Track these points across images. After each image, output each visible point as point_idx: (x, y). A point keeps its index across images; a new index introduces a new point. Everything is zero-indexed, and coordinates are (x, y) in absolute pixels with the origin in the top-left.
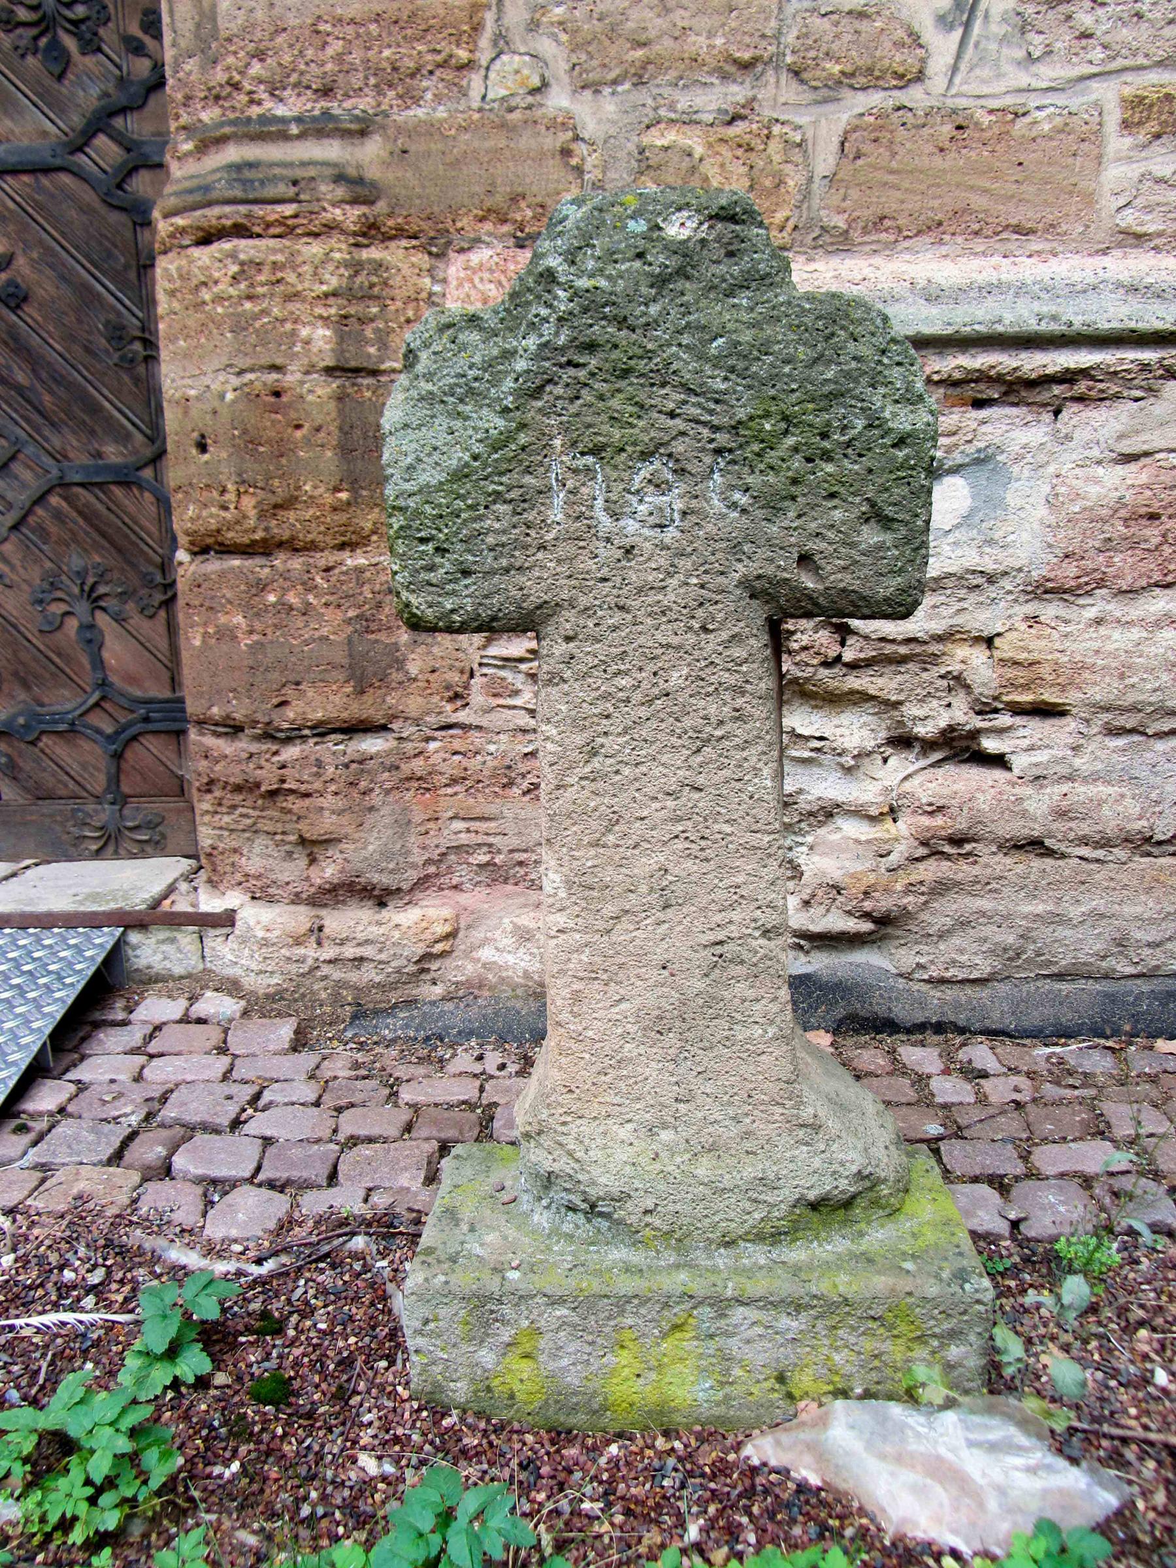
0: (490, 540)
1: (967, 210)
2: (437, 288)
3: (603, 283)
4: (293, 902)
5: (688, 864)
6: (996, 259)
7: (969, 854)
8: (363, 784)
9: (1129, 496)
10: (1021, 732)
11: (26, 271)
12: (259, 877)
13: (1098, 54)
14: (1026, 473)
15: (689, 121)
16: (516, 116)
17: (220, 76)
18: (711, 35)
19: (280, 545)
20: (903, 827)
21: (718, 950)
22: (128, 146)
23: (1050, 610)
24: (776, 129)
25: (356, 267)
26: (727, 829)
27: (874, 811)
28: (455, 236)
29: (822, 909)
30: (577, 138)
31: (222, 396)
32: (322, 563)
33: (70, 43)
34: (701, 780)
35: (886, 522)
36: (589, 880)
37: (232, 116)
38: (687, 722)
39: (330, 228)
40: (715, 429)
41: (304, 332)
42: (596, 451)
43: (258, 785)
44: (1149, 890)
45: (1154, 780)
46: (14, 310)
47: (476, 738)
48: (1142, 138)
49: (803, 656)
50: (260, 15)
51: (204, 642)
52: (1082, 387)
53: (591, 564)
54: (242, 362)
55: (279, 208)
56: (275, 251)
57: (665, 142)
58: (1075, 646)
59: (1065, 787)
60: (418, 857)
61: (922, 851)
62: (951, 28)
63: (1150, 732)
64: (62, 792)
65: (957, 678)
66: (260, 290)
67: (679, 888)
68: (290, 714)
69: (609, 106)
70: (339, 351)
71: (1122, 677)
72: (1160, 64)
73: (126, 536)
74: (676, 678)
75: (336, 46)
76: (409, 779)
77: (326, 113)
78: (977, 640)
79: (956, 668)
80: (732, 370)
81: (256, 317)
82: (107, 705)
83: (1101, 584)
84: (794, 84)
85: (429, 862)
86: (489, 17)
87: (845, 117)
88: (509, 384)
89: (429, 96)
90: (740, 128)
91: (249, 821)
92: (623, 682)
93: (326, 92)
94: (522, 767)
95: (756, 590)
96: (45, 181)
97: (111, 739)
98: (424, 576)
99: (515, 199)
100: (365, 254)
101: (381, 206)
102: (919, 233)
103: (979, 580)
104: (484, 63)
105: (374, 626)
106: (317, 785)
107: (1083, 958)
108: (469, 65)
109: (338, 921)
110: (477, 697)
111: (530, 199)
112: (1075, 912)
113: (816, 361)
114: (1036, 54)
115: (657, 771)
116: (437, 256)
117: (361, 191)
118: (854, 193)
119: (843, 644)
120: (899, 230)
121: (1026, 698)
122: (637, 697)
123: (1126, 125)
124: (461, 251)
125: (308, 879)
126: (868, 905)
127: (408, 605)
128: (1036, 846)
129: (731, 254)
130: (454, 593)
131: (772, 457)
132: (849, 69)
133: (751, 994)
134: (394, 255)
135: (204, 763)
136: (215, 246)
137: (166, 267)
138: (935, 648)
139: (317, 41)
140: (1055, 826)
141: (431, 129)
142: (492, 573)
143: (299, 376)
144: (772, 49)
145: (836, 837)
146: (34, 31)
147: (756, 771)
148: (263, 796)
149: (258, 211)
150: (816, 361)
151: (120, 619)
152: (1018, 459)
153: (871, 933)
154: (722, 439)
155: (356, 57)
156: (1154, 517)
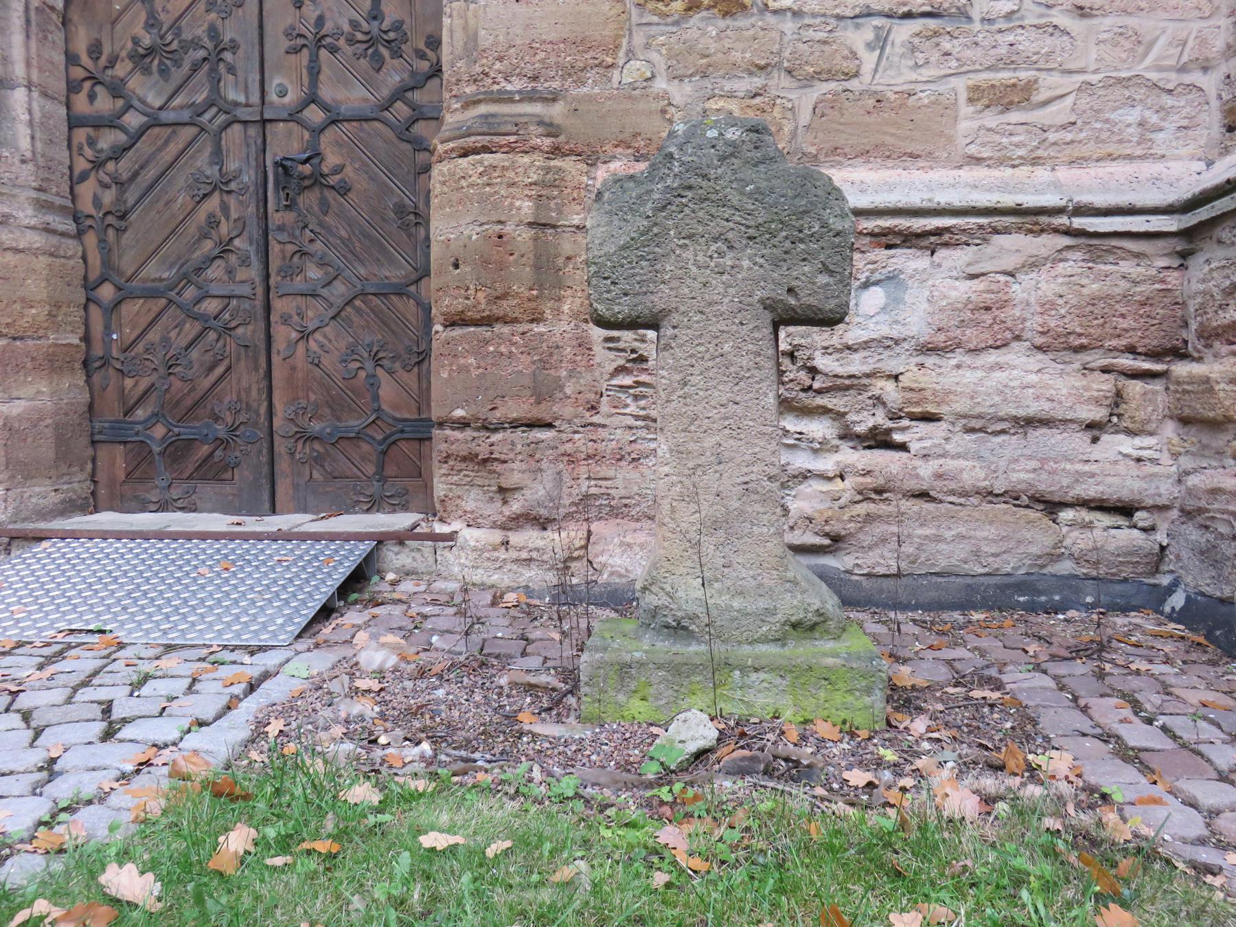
0: (638, 278)
1: (883, 144)
2: (590, 182)
3: (695, 159)
5: (731, 442)
6: (900, 171)
7: (886, 499)
8: (537, 456)
9: (974, 297)
10: (915, 430)
11: (351, 175)
13: (954, 64)
14: (916, 285)
15: (731, 95)
16: (637, 92)
17: (478, 69)
18: (743, 52)
19: (497, 319)
20: (848, 483)
21: (746, 486)
23: (930, 361)
24: (778, 101)
25: (548, 170)
26: (751, 423)
27: (831, 474)
28: (601, 155)
29: (801, 531)
30: (670, 104)
31: (470, 237)
32: (521, 330)
33: (385, 52)
34: (738, 399)
35: (831, 273)
36: (682, 448)
37: (482, 90)
38: (732, 369)
39: (534, 148)
40: (748, 227)
41: (518, 203)
42: (690, 237)
43: (477, 456)
44: (991, 523)
45: (992, 459)
46: (342, 196)
47: (602, 433)
48: (979, 106)
49: (791, 385)
50: (501, 38)
52: (946, 237)
53: (686, 291)
54: (483, 219)
56: (503, 160)
57: (717, 107)
58: (945, 380)
59: (942, 461)
60: (566, 501)
61: (859, 497)
62: (873, 49)
63: (989, 430)
64: (349, 473)
65: (878, 398)
66: (495, 181)
67: (726, 454)
68: (498, 414)
69: (688, 88)
70: (536, 214)
71: (972, 398)
72: (988, 69)
73: (397, 324)
74: (727, 347)
75: (542, 55)
76: (563, 455)
77: (534, 89)
78: (889, 377)
79: (877, 392)
80: (756, 200)
81: (492, 195)
82: (379, 422)
83: (959, 345)
84: (789, 78)
85: (573, 504)
86: (625, 42)
87: (816, 95)
88: (650, 205)
90: (758, 100)
92: (702, 349)
93: (535, 78)
94: (628, 449)
95: (768, 305)
96: (365, 125)
97: (380, 443)
98: (605, 295)
99: (635, 135)
100: (552, 163)
101: (562, 138)
102: (857, 156)
103: (890, 343)
104: (621, 64)
105: (547, 366)
106: (511, 456)
107: (954, 562)
108: (612, 66)
109: (516, 538)
110: (605, 407)
111: (643, 136)
112: (948, 534)
113: (796, 196)
114: (920, 63)
115: (717, 393)
116: (591, 165)
117: (550, 129)
118: (820, 135)
119: (813, 379)
120: (846, 155)
121: (917, 410)
122: (707, 356)
123: (971, 100)
124: (605, 162)
125: (501, 513)
126: (827, 529)
127: (596, 310)
128: (923, 495)
129: (756, 148)
130: (619, 304)
131: (775, 241)
132: (818, 70)
133: (762, 510)
134: (568, 164)
135: (445, 445)
136: (471, 158)
137: (440, 171)
138: (865, 381)
139: (532, 52)
140: (935, 483)
141: (590, 99)
142: (638, 294)
144: (776, 59)
145: (809, 490)
146: (366, 46)
147: (766, 395)
148: (478, 464)
149: (496, 139)
150: (796, 196)
151: (391, 372)
152: (911, 277)
153: (829, 546)
154: (751, 232)
155: (552, 60)
156: (988, 309)
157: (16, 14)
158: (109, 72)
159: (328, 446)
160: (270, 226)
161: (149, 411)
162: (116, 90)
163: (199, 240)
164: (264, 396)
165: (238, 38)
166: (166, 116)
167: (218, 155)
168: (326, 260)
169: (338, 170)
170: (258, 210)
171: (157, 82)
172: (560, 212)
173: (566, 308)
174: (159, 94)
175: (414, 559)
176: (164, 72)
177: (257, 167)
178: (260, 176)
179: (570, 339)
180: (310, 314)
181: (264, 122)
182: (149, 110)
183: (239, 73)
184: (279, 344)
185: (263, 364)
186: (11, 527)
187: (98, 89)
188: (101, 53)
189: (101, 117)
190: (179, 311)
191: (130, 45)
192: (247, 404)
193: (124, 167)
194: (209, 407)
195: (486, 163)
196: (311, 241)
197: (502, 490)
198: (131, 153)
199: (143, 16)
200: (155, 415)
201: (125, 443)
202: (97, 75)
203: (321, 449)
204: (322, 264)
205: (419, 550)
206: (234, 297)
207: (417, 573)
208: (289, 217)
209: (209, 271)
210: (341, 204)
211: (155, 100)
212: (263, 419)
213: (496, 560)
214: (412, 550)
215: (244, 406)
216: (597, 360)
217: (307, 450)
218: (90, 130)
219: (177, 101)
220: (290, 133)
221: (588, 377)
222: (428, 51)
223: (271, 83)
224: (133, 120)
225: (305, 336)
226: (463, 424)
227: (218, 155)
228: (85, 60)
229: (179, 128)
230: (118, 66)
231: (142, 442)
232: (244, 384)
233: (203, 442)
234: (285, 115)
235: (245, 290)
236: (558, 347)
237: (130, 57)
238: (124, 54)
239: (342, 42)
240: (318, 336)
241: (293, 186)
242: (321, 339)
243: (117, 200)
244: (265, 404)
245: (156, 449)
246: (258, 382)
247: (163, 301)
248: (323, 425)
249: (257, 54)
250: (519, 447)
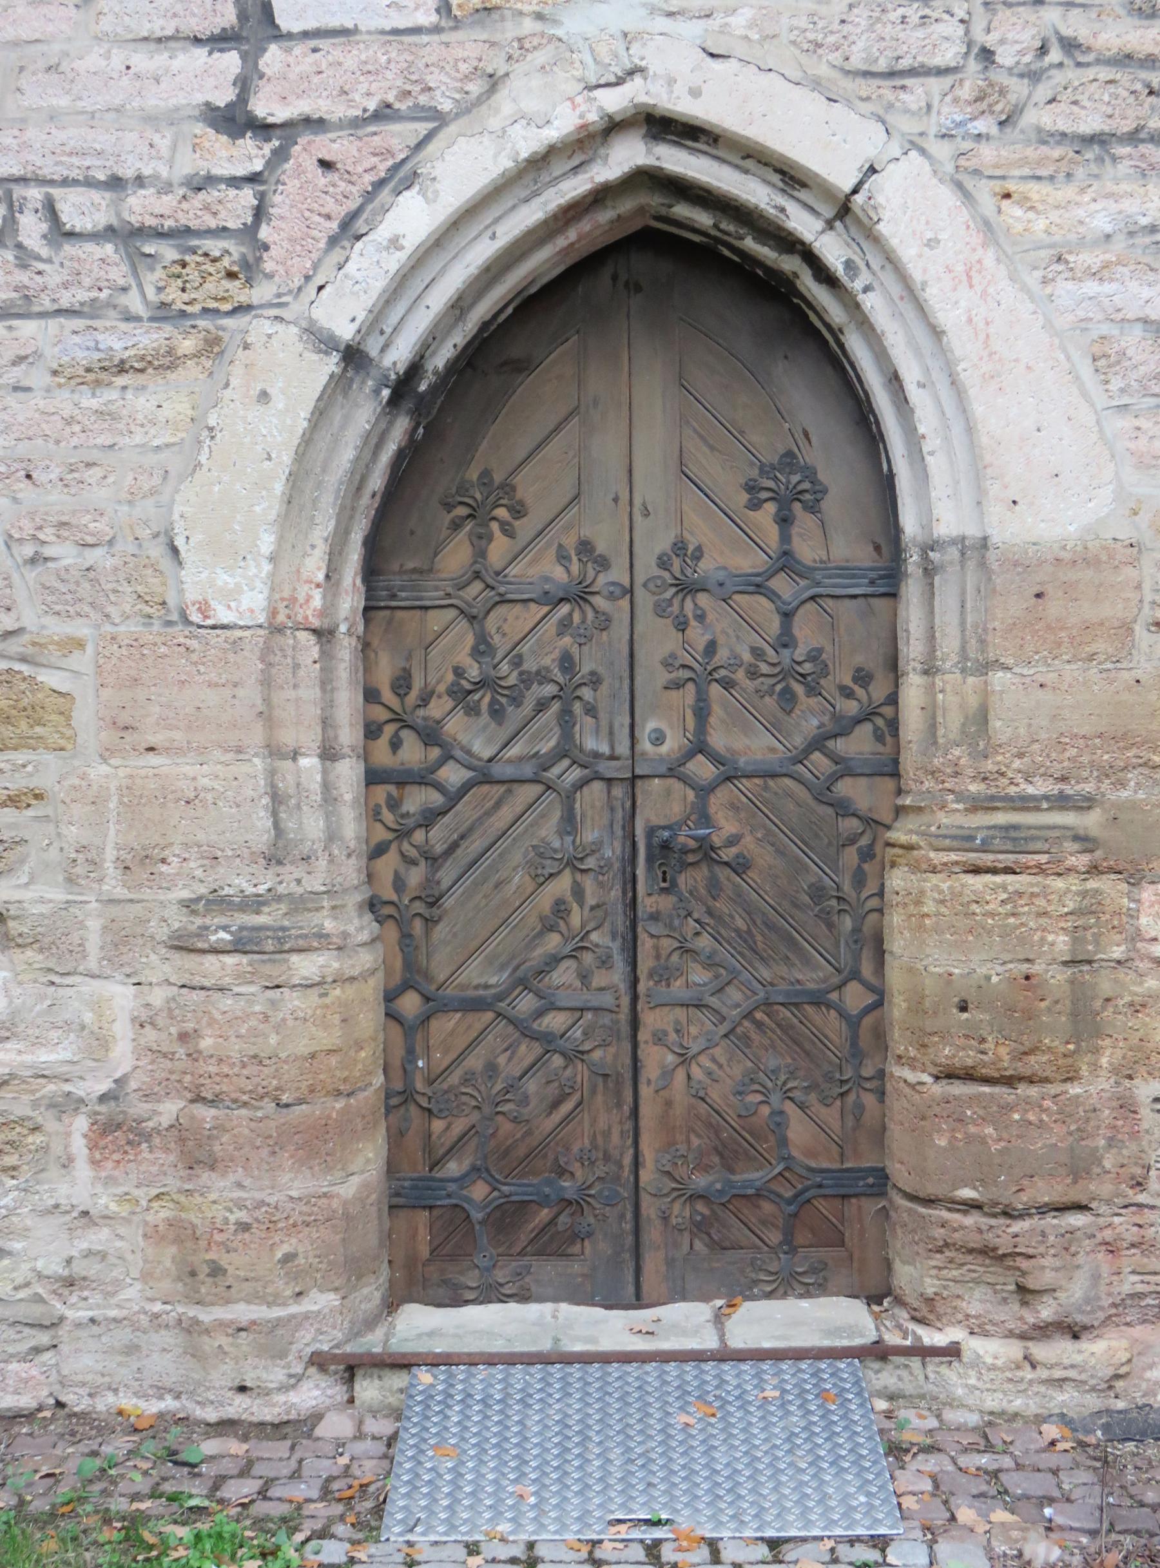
2: (1132, 905)
4: (1006, 1337)
8: (1073, 1249)
12: (976, 1317)
19: (1021, 1079)
22: (836, 759)
25: (1084, 894)
28: (1147, 873)
31: (988, 978)
32: (1053, 1092)
33: (799, 689)
41: (1050, 938)
50: (1022, 731)
51: (950, 1142)
55: (1036, 857)
60: (1106, 1302)
70: (1073, 951)
77: (1061, 792)
81: (1017, 927)
85: (1114, 1305)
89: (1132, 783)
91: (974, 1275)
93: (1064, 779)
96: (771, 783)
97: (789, 1202)
101: (1099, 854)
105: (1084, 1135)
106: (1042, 1249)
109: (1040, 1351)
117: (1090, 846)
125: (1021, 1318)
135: (942, 1230)
141: (1133, 806)
143: (1044, 966)
149: (1023, 858)
151: (802, 1107)
155: (1085, 759)
157: (343, 666)
158: (421, 712)
159: (715, 1207)
160: (640, 914)
161: (466, 1164)
162: (430, 736)
163: (540, 934)
164: (630, 1142)
165: (601, 670)
166: (497, 770)
167: (570, 824)
168: (717, 959)
169: (733, 841)
170: (624, 893)
171: (485, 728)
172: (1097, 943)
173: (1104, 1061)
174: (489, 741)
175: (900, 1379)
176: (497, 713)
177: (624, 837)
178: (628, 850)
179: (1110, 1099)
180: (694, 1030)
181: (635, 777)
182: (476, 763)
183: (603, 715)
184: (651, 1071)
185: (629, 1099)
186: (348, 1349)
187: (405, 734)
188: (409, 688)
189: (409, 772)
190: (511, 1028)
191: (450, 677)
192: (605, 1153)
193: (438, 836)
194: (551, 1156)
195: (1011, 889)
196: (697, 934)
197: (1021, 1289)
198: (447, 819)
199: (470, 640)
200: (475, 1169)
201: (431, 1208)
202: (405, 717)
203: (706, 1212)
204: (710, 963)
205: (906, 1366)
206: (589, 1009)
207: (904, 1397)
208: (665, 903)
209: (555, 975)
210: (739, 886)
211: (482, 749)
212: (626, 1172)
213: (1022, 1380)
214: (898, 1367)
215: (601, 1155)
216: (1145, 1125)
217: (687, 1213)
218: (392, 788)
219: (514, 751)
220: (668, 792)
221: (1134, 1147)
222: (856, 688)
223: (644, 727)
224: (453, 775)
225: (685, 1059)
226: (974, 1206)
227: (570, 824)
228: (388, 696)
229: (515, 786)
230: (433, 703)
231: (456, 1206)
232: (602, 1124)
233: (540, 1205)
234: (663, 769)
235: (607, 1000)
236: (1095, 1110)
237: (451, 693)
238: (442, 688)
239: (740, 675)
240: (704, 1060)
241: (673, 862)
242: (708, 1064)
243: (428, 880)
244: (631, 1151)
245: (477, 1215)
246: (621, 1122)
247: (490, 1015)
248: (711, 1178)
249: (626, 690)
250: (1052, 1238)
